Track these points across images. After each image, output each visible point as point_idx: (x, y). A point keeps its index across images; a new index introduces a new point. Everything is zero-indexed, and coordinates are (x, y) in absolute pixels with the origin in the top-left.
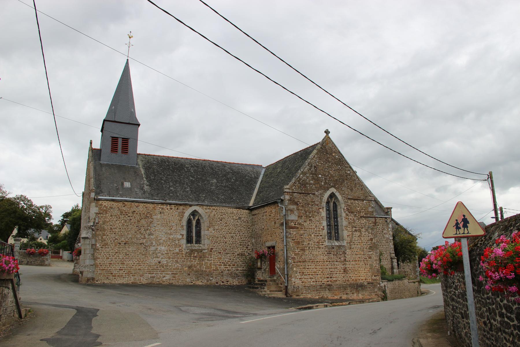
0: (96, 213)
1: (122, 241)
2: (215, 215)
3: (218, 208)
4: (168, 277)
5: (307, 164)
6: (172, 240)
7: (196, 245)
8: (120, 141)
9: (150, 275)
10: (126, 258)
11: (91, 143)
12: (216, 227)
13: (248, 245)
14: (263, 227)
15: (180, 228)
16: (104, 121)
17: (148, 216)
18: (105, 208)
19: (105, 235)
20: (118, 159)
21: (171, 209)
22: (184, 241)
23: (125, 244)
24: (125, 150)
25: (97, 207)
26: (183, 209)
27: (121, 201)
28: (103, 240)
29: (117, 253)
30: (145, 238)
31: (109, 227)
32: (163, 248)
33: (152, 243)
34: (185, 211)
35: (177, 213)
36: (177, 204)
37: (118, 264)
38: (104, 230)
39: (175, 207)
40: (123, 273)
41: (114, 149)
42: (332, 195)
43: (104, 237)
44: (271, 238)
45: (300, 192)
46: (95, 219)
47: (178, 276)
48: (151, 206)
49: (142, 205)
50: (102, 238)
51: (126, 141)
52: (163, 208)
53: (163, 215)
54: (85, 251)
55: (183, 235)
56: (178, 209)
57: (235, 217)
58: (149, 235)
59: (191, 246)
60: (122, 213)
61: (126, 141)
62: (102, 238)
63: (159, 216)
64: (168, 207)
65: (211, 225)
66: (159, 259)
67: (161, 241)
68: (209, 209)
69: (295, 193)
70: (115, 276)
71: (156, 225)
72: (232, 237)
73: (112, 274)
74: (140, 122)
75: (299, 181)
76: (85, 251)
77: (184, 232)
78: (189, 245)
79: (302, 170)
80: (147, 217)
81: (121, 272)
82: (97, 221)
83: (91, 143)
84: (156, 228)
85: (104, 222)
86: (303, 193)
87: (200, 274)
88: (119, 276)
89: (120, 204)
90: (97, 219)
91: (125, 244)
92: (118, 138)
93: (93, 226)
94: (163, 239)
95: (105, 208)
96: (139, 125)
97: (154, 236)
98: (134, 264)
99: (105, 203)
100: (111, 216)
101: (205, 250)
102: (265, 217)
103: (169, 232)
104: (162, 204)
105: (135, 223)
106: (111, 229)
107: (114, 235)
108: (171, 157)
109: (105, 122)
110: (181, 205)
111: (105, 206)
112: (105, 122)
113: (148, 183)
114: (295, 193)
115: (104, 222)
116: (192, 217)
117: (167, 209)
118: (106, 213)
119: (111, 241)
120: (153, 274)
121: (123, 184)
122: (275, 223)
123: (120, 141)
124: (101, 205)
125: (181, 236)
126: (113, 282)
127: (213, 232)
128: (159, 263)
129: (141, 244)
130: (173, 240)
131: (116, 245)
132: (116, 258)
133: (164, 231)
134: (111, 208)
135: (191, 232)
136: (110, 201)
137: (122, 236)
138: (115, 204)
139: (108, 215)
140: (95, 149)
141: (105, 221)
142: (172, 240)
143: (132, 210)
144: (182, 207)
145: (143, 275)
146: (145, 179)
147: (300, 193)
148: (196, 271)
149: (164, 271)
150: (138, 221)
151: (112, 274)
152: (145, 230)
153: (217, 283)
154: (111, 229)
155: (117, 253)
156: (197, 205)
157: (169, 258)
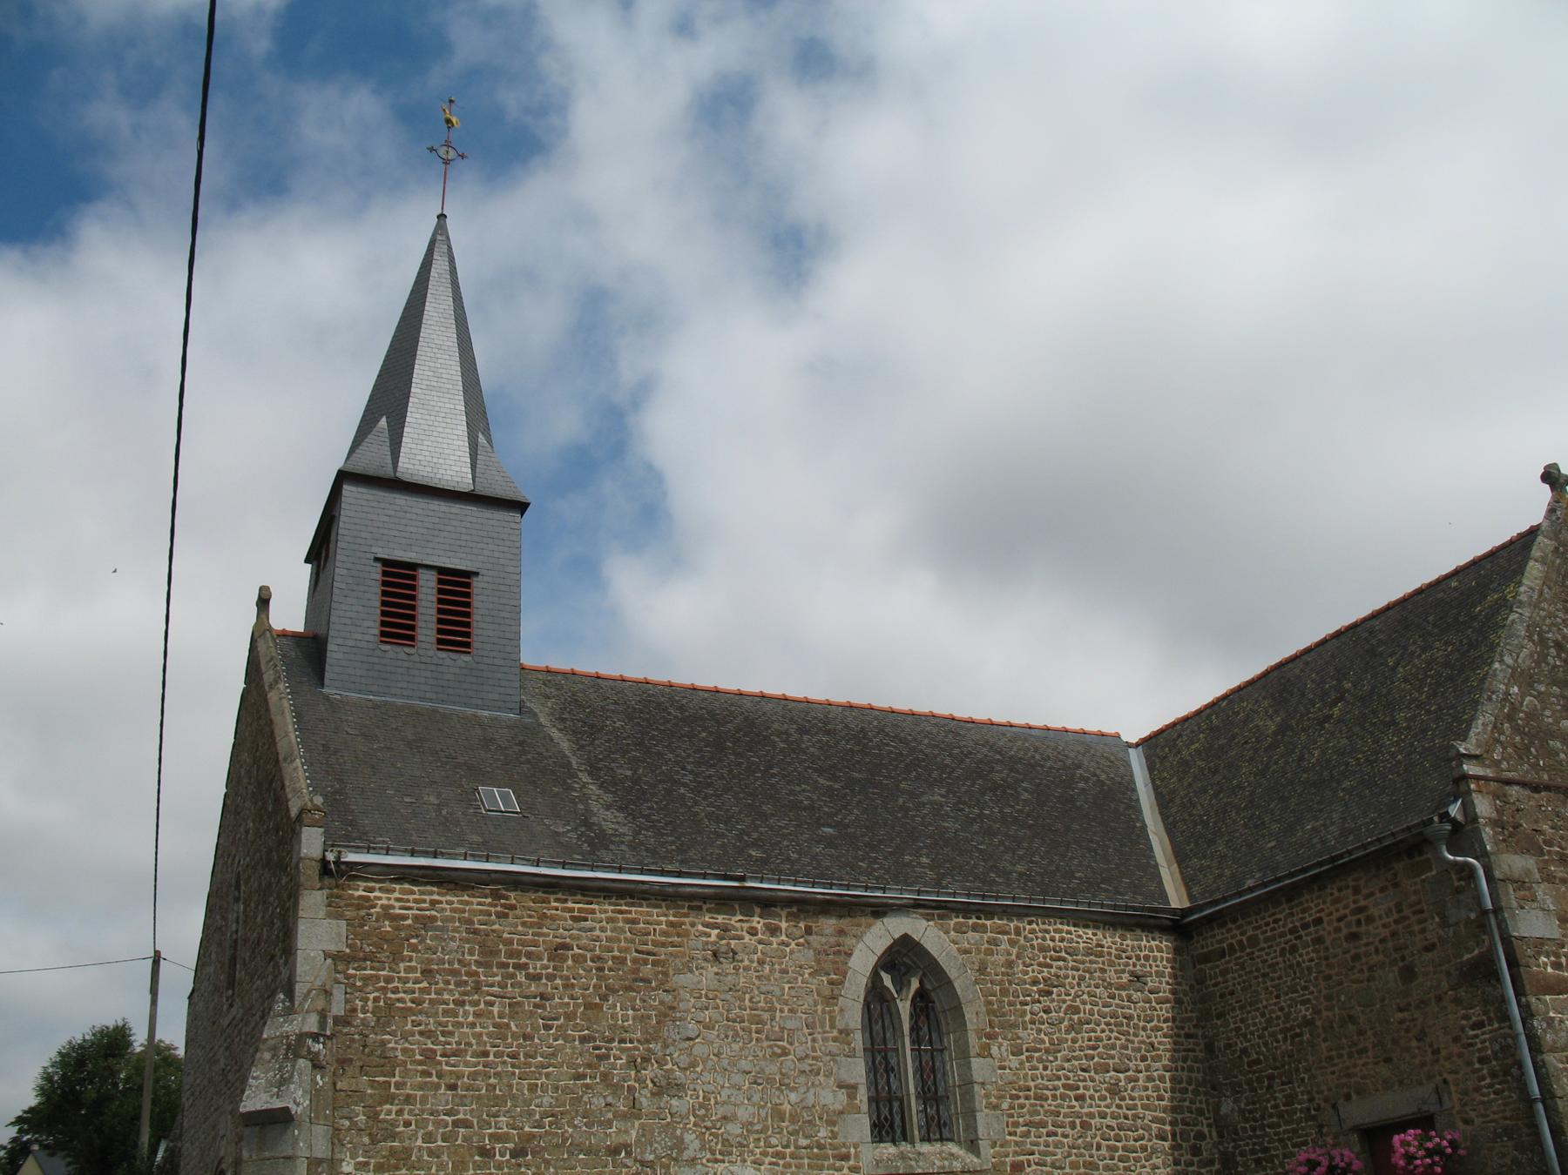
0: (337, 957)
1: (495, 1138)
2: (1010, 964)
5: (1521, 630)
6: (794, 1118)
7: (926, 1148)
8: (427, 587)
11: (264, 602)
12: (1028, 1035)
13: (1200, 1136)
14: (1305, 1012)
15: (833, 1047)
16: (343, 477)
18: (387, 927)
19: (391, 1099)
20: (423, 668)
21: (774, 931)
22: (859, 1127)
23: (518, 1153)
24: (456, 630)
26: (841, 932)
30: (634, 1111)
31: (417, 1044)
33: (680, 1145)
34: (849, 941)
38: (387, 1063)
41: (397, 625)
43: (388, 1112)
44: (1384, 1070)
45: (1531, 777)
46: (328, 993)
48: (659, 918)
49: (603, 910)
50: (373, 1117)
51: (455, 584)
52: (725, 929)
53: (728, 967)
55: (852, 1089)
56: (809, 931)
57: (1111, 975)
58: (658, 1093)
59: (903, 1157)
60: (488, 952)
62: (373, 1117)
63: (707, 976)
64: (758, 922)
65: (1000, 1023)
67: (734, 1129)
68: (975, 928)
69: (1509, 782)
72: (1114, 1090)
75: (1510, 718)
77: (857, 1071)
78: (889, 1150)
79: (1508, 660)
80: (635, 982)
82: (338, 1008)
83: (264, 602)
85: (387, 1014)
86: (1547, 788)
89: (476, 903)
90: (339, 994)
92: (414, 566)
93: (315, 1037)
94: (743, 1113)
95: (387, 927)
97: (689, 1100)
99: (387, 898)
100: (427, 973)
102: (1306, 955)
103: (772, 1069)
104: (722, 901)
105: (570, 1017)
106: (429, 1056)
108: (685, 688)
109: (348, 490)
110: (827, 907)
111: (386, 913)
112: (348, 490)
113: (608, 798)
114: (1509, 782)
116: (887, 980)
117: (753, 932)
118: (397, 957)
119: (429, 1138)
121: (470, 798)
122: (1408, 973)
123: (427, 587)
124: (366, 903)
125: (842, 1096)
127: (1014, 1062)
129: (614, 1151)
130: (802, 1120)
133: (744, 1064)
134: (425, 922)
135: (920, 1070)
138: (450, 902)
139: (408, 969)
140: (284, 634)
141: (390, 1005)
142: (794, 1118)
143: (550, 935)
144: (829, 924)
146: (585, 778)
147: (1536, 789)
150: (588, 1006)
152: (632, 1062)
154: (429, 1056)
156: (917, 905)
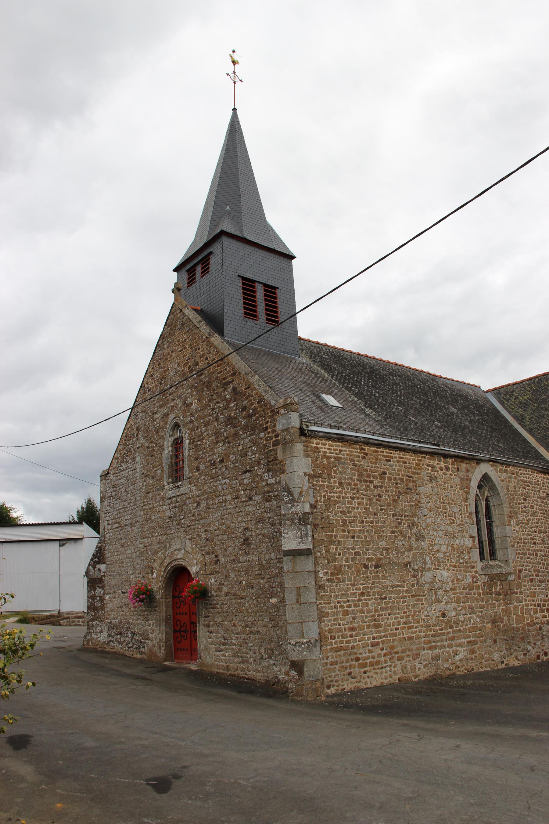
3: (515, 470)
4: (463, 653)
8: (260, 291)
9: (430, 652)
10: (383, 609)
17: (409, 487)
25: (307, 456)
27: (356, 442)
28: (331, 559)
29: (362, 594)
32: (445, 574)
33: (425, 563)
35: (457, 481)
36: (456, 457)
37: (368, 627)
39: (453, 464)
40: (379, 655)
42: (486, 478)
47: (480, 648)
49: (396, 454)
50: (328, 551)
53: (435, 484)
54: (298, 595)
56: (458, 469)
61: (271, 291)
62: (328, 551)
66: (442, 606)
67: (441, 555)
70: (365, 665)
71: (425, 511)
73: (358, 659)
74: (293, 249)
76: (298, 595)
81: (377, 651)
84: (429, 521)
87: (513, 637)
88: (372, 664)
89: (355, 451)
91: (376, 567)
92: (254, 281)
94: (443, 548)
96: (293, 257)
98: (399, 623)
100: (341, 484)
101: (510, 574)
104: (432, 454)
107: (350, 543)
115: (329, 503)
120: (435, 647)
123: (260, 291)
126: (362, 685)
128: (444, 615)
131: (358, 573)
132: (362, 612)
136: (333, 440)
137: (368, 543)
138: (346, 450)
144: (464, 466)
145: (418, 655)
148: (506, 631)
149: (453, 639)
151: (358, 659)
153: (538, 657)
155: (362, 594)
157: (458, 601)
